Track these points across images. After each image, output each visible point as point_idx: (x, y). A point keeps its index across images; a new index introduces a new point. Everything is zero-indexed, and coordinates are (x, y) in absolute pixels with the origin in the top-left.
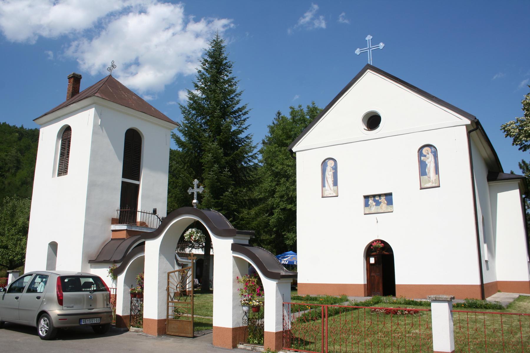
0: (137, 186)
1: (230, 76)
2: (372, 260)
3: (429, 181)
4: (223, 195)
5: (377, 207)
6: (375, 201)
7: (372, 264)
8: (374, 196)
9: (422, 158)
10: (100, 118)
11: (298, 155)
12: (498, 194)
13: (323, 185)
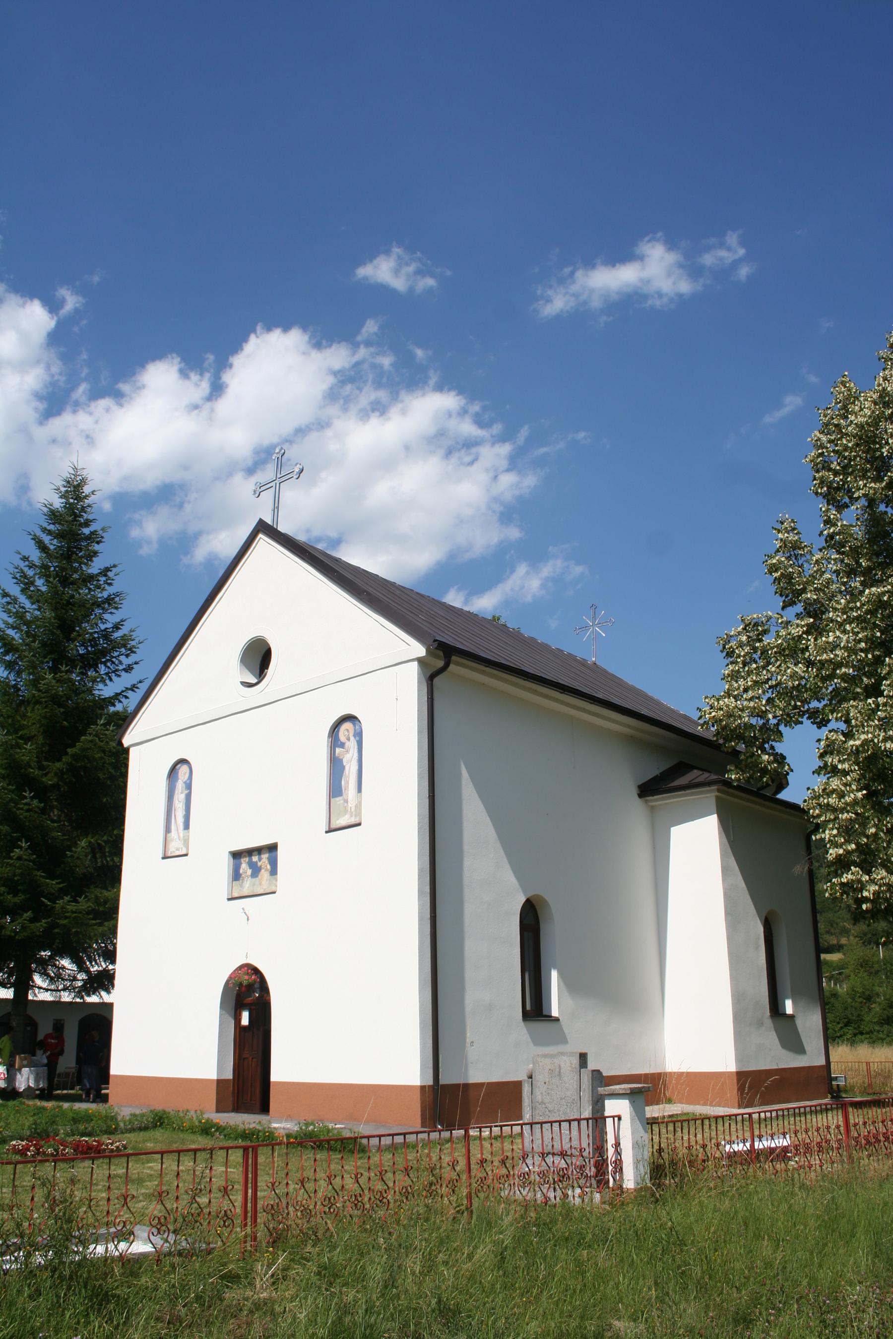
1: (110, 590)
2: (245, 1020)
3: (346, 811)
4: (71, 851)
5: (254, 880)
6: (252, 865)
7: (245, 1027)
8: (250, 852)
9: (338, 750)
11: (132, 751)
13: (168, 830)
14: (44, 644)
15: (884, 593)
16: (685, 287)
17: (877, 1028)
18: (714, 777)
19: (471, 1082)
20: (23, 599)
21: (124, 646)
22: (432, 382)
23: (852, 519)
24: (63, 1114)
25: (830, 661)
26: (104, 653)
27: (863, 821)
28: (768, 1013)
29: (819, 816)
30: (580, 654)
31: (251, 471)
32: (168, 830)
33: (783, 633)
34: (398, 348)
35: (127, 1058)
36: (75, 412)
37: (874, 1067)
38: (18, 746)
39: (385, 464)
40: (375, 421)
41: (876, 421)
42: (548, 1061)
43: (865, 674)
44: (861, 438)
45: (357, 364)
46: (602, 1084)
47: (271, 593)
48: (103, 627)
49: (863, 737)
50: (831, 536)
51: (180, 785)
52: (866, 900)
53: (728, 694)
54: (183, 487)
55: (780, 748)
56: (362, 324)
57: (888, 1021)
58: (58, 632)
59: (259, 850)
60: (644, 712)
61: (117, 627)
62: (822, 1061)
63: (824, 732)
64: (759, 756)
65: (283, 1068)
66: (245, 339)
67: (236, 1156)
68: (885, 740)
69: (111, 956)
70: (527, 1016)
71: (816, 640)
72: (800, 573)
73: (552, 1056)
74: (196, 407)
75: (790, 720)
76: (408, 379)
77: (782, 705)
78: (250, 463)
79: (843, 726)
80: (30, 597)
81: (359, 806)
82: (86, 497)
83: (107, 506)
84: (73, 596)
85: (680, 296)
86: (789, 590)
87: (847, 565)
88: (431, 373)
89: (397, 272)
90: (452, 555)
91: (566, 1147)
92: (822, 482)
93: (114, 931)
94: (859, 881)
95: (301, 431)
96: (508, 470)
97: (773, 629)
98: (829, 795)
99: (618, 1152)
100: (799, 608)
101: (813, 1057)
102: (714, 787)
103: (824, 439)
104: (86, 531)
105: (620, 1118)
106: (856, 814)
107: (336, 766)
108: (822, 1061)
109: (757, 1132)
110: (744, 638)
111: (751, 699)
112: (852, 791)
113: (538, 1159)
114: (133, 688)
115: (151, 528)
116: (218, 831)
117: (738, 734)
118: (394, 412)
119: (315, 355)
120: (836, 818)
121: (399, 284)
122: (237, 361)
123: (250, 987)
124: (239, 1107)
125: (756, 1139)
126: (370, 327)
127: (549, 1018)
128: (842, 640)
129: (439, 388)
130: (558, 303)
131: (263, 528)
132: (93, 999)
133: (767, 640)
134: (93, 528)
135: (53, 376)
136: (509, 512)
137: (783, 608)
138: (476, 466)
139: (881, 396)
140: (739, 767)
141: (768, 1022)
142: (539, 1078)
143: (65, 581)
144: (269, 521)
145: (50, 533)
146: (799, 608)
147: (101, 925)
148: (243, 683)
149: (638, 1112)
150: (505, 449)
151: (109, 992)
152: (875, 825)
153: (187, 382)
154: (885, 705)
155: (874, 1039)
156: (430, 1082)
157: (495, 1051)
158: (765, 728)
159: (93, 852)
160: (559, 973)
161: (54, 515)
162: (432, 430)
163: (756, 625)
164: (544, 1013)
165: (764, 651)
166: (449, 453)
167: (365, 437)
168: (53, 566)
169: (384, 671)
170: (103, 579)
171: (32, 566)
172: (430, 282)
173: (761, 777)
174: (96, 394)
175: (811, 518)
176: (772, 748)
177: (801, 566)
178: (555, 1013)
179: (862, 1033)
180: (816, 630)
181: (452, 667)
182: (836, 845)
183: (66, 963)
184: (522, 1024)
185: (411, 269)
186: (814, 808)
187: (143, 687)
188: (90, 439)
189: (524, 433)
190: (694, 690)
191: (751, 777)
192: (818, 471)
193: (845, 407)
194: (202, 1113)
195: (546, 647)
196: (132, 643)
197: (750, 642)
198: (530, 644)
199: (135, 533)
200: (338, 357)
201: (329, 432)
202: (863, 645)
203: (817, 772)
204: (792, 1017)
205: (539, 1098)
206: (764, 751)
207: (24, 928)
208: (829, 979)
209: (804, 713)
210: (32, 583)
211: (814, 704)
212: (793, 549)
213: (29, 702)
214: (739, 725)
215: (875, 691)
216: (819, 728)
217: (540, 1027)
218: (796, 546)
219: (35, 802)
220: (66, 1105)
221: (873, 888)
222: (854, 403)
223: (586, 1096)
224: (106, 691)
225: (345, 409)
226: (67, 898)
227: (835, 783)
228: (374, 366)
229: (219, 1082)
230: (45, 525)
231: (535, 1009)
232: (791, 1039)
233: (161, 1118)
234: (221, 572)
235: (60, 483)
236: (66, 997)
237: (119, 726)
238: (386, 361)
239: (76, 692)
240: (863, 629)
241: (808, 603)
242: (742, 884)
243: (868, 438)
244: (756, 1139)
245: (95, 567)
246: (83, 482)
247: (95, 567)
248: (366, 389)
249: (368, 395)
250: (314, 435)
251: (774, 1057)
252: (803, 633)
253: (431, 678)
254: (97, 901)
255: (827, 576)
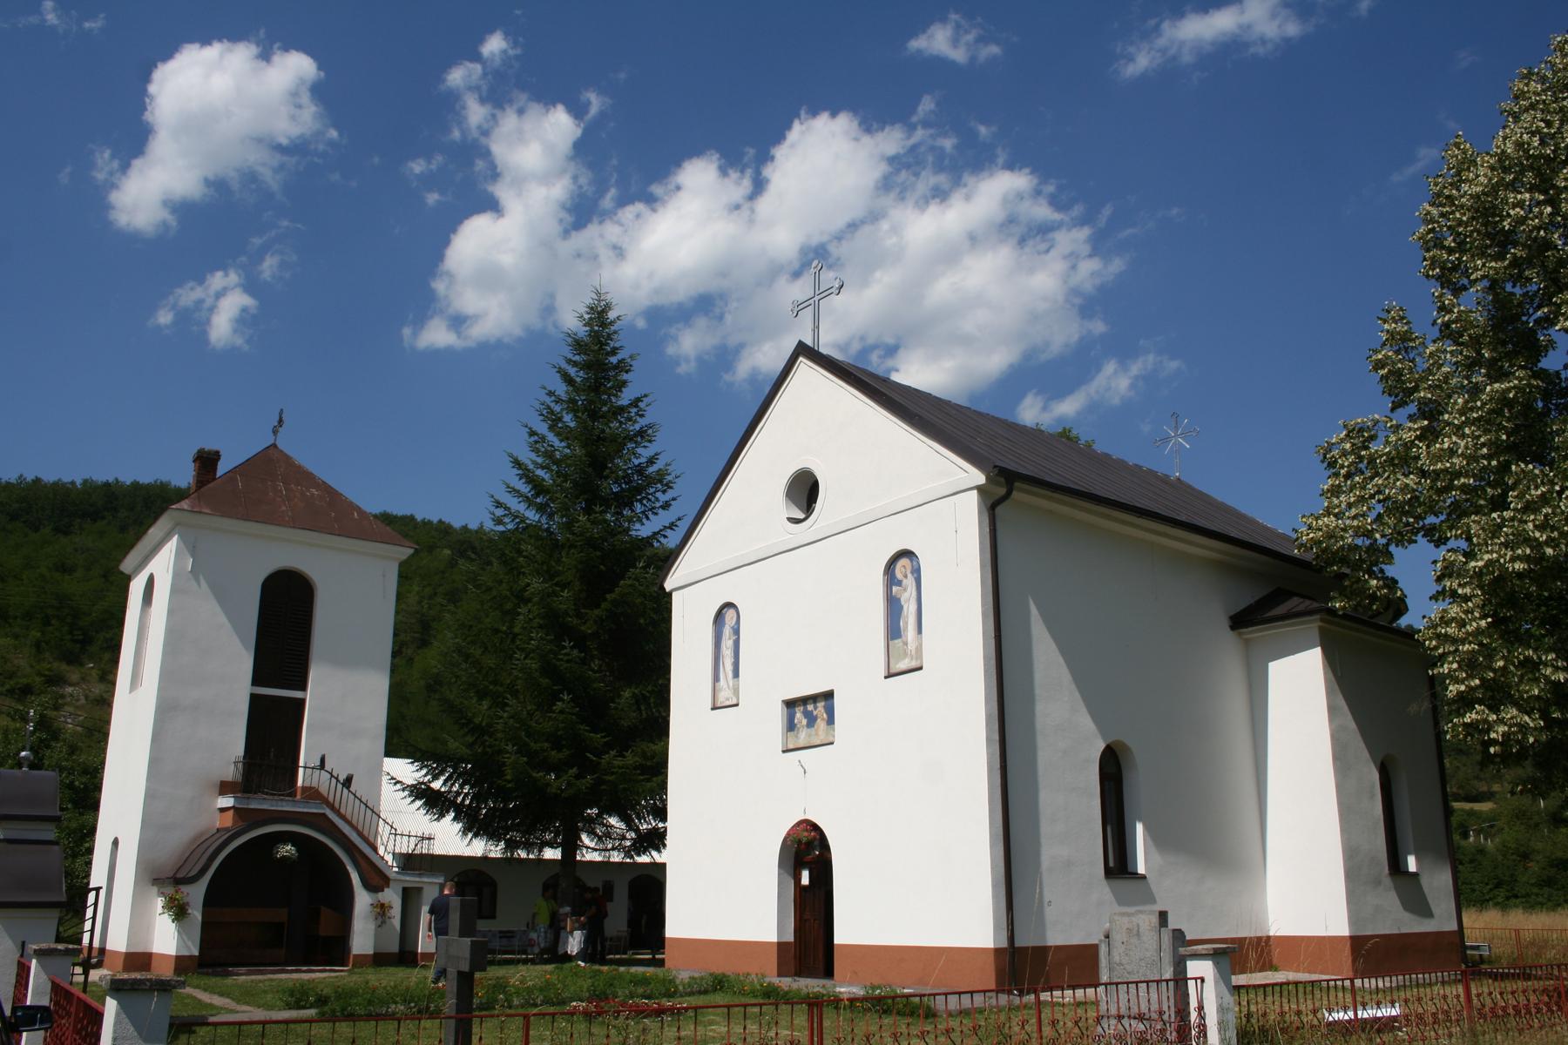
0: (302, 702)
1: (642, 422)
2: (805, 879)
3: (905, 654)
6: (807, 714)
8: (804, 701)
10: (193, 556)
11: (676, 599)
12: (1272, 665)
13: (716, 678)
14: (575, 483)
15: (1509, 390)
16: (1293, 29)
17: (1535, 890)
18: (1316, 605)
19: (1050, 943)
20: (551, 437)
21: (660, 481)
22: (1000, 161)
23: (1472, 304)
24: (621, 976)
25: (1446, 470)
26: (639, 490)
27: (1490, 654)
28: (1386, 870)
29: (1436, 648)
30: (1161, 469)
31: (797, 275)
32: (716, 678)
33: (1393, 438)
34: (949, 128)
35: (685, 918)
36: (601, 223)
37: (1527, 936)
38: (555, 594)
39: (947, 256)
40: (933, 208)
41: (1493, 190)
42: (1125, 919)
43: (1489, 484)
44: (1477, 211)
45: (913, 149)
46: (1182, 947)
47: (815, 419)
48: (636, 462)
49: (1487, 557)
50: (1447, 325)
51: (727, 631)
52: (1494, 742)
53: (1328, 512)
54: (723, 296)
55: (1390, 571)
56: (918, 101)
57: (1549, 882)
58: (590, 470)
59: (814, 699)
60: (1234, 533)
61: (651, 461)
62: (1454, 926)
63: (1442, 552)
64: (1366, 581)
65: (848, 929)
66: (789, 127)
67: (801, 1019)
68: (1513, 560)
69: (662, 814)
70: (1109, 873)
71: (1428, 447)
72: (1411, 371)
73: (1129, 915)
74: (737, 207)
75: (1402, 537)
76: (968, 161)
77: (1391, 522)
78: (796, 265)
79: (1463, 544)
80: (558, 434)
81: (919, 649)
82: (612, 323)
83: (641, 323)
84: (603, 431)
85: (1287, 41)
86: (1399, 389)
87: (1467, 357)
88: (999, 151)
89: (955, 42)
90: (1028, 356)
91: (1144, 1009)
92: (1434, 262)
93: (663, 787)
94: (1485, 721)
95: (853, 226)
96: (1090, 256)
97: (1381, 435)
98: (1447, 624)
99: (1202, 1016)
100: (1412, 408)
101: (1442, 919)
102: (1318, 617)
103: (1435, 212)
104: (614, 360)
105: (1203, 980)
106: (1481, 644)
107: (893, 607)
108: (1454, 926)
109: (1359, 999)
110: (1348, 446)
111: (1354, 518)
112: (1474, 619)
113: (1113, 1022)
114: (672, 526)
115: (690, 343)
116: (770, 677)
117: (1342, 557)
118: (957, 201)
119: (867, 140)
120: (1457, 650)
121: (959, 55)
122: (780, 152)
123: (809, 845)
124: (800, 972)
125: (1360, 1007)
126: (927, 105)
127: (1135, 875)
128: (1459, 445)
129: (1010, 166)
130: (1142, 61)
131: (803, 350)
132: (644, 859)
133: (1374, 447)
134: (619, 356)
135: (580, 187)
136: (1088, 304)
137: (1393, 410)
138: (1053, 253)
139: (1500, 160)
140: (1344, 594)
141: (1387, 881)
142: (1117, 937)
143: (594, 415)
144: (809, 342)
145: (575, 364)
146: (1412, 408)
147: (648, 780)
148: (790, 519)
149: (1223, 976)
150: (1085, 232)
151: (659, 851)
152: (1503, 657)
153: (726, 180)
154: (1512, 519)
155: (1531, 903)
156: (1004, 944)
157: (1074, 911)
158: (1372, 548)
159: (637, 702)
160: (1146, 828)
161: (578, 345)
162: (1000, 216)
163: (1361, 430)
164: (1130, 869)
165: (1372, 460)
166: (1022, 241)
167: (926, 226)
168: (581, 400)
169: (934, 503)
170: (634, 410)
171: (558, 401)
172: (994, 49)
173: (1371, 604)
174: (624, 201)
175: (1422, 304)
176: (1382, 571)
177: (1413, 361)
178: (1141, 869)
179: (1516, 897)
180: (1430, 435)
181: (1015, 494)
182: (1457, 681)
183: (613, 821)
184: (1104, 882)
185: (970, 37)
186: (1430, 639)
187: (683, 526)
188: (619, 252)
189: (1107, 211)
190: (1291, 505)
191: (1359, 604)
192: (1428, 250)
193: (1458, 174)
194: (764, 976)
195: (1121, 464)
196: (669, 478)
197: (1355, 450)
198: (1105, 461)
199: (671, 350)
200: (891, 141)
201: (885, 226)
202: (1485, 450)
203: (1434, 598)
204: (1415, 875)
205: (1117, 959)
206: (1372, 574)
207: (569, 784)
208: (1478, 833)
209: (1418, 530)
210: (560, 419)
211: (1431, 520)
212: (1402, 341)
213: (563, 546)
214: (1342, 547)
215: (1500, 504)
216: (1437, 546)
217: (1125, 885)
218: (1406, 337)
219: (575, 652)
220: (622, 969)
221: (1502, 729)
222: (1468, 169)
223: (1167, 957)
224: (643, 530)
225: (902, 198)
226: (613, 753)
227: (1454, 611)
228: (932, 149)
229: (779, 944)
230: (570, 356)
231: (1119, 865)
232: (1415, 901)
233: (720, 982)
234: (767, 390)
235: (582, 310)
236: (616, 857)
237: (659, 568)
238: (948, 144)
239: (613, 533)
240: (1486, 432)
241: (1423, 403)
242: (1352, 725)
243: (1486, 210)
244: (1360, 1007)
245: (625, 398)
246: (608, 307)
247: (625, 398)
248: (924, 173)
249: (928, 179)
250: (866, 230)
251: (1395, 920)
252: (1417, 438)
253: (993, 504)
254: (644, 755)
255: (1446, 369)
